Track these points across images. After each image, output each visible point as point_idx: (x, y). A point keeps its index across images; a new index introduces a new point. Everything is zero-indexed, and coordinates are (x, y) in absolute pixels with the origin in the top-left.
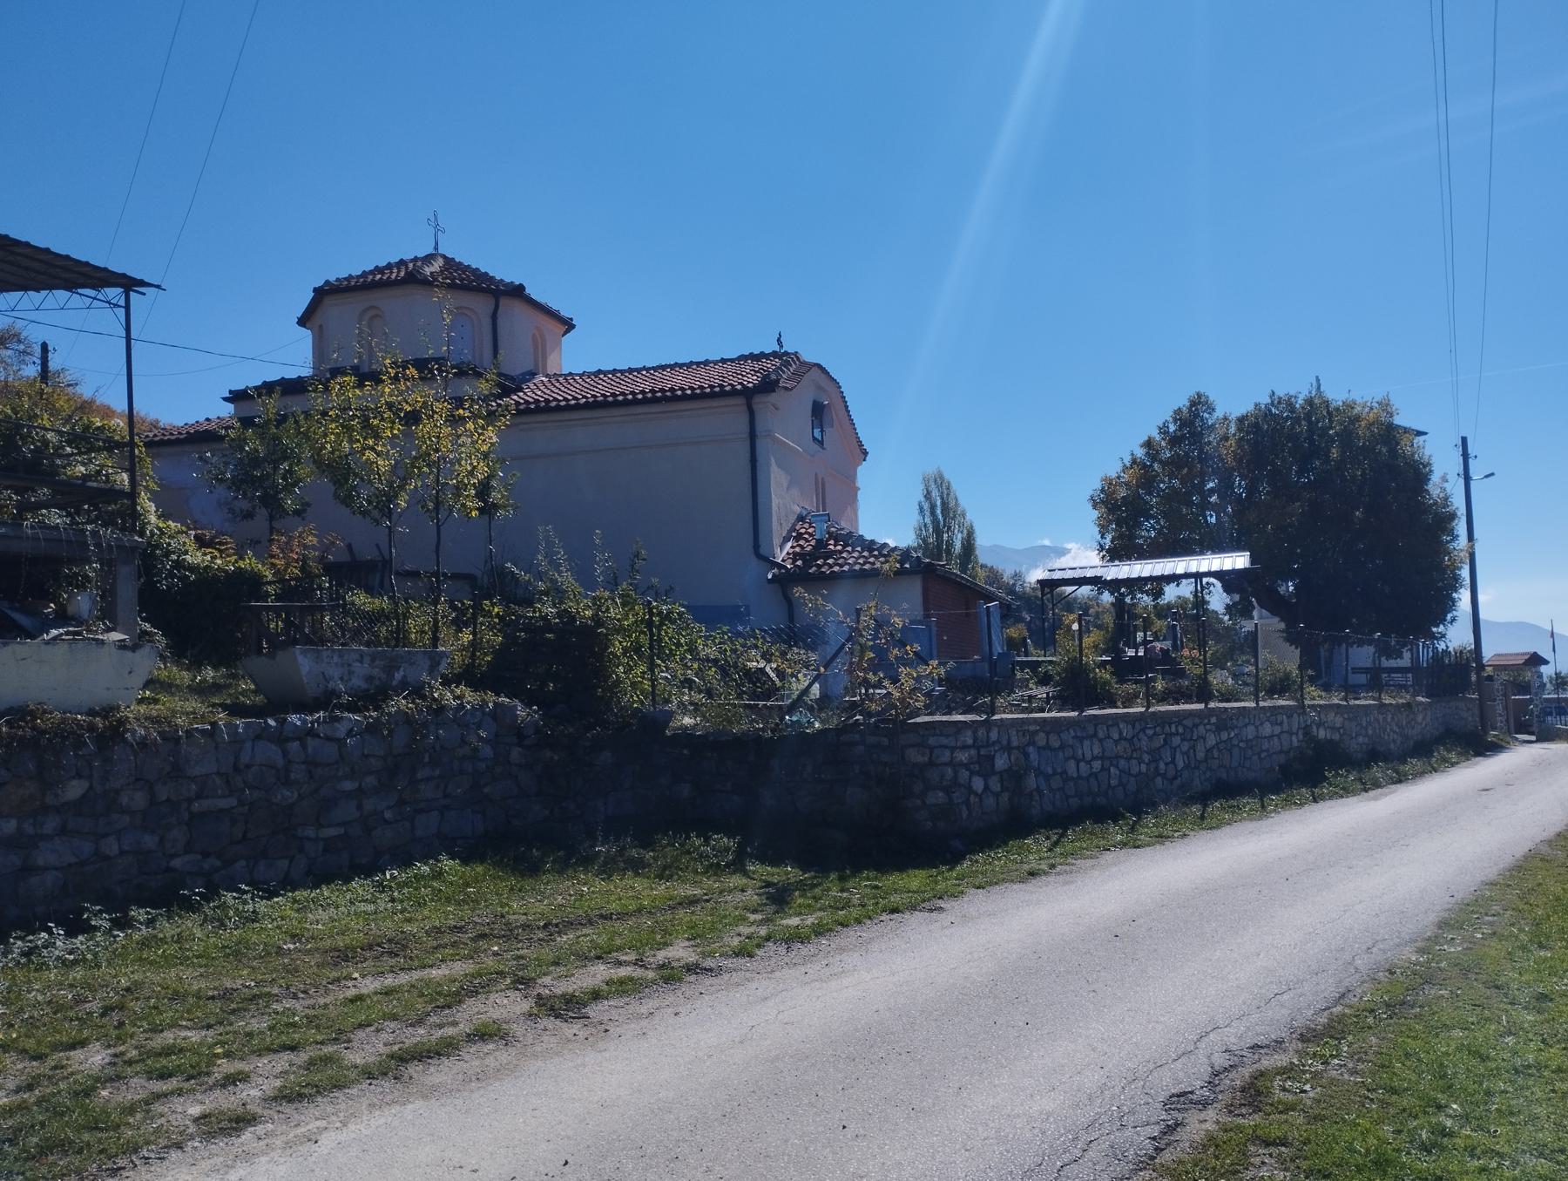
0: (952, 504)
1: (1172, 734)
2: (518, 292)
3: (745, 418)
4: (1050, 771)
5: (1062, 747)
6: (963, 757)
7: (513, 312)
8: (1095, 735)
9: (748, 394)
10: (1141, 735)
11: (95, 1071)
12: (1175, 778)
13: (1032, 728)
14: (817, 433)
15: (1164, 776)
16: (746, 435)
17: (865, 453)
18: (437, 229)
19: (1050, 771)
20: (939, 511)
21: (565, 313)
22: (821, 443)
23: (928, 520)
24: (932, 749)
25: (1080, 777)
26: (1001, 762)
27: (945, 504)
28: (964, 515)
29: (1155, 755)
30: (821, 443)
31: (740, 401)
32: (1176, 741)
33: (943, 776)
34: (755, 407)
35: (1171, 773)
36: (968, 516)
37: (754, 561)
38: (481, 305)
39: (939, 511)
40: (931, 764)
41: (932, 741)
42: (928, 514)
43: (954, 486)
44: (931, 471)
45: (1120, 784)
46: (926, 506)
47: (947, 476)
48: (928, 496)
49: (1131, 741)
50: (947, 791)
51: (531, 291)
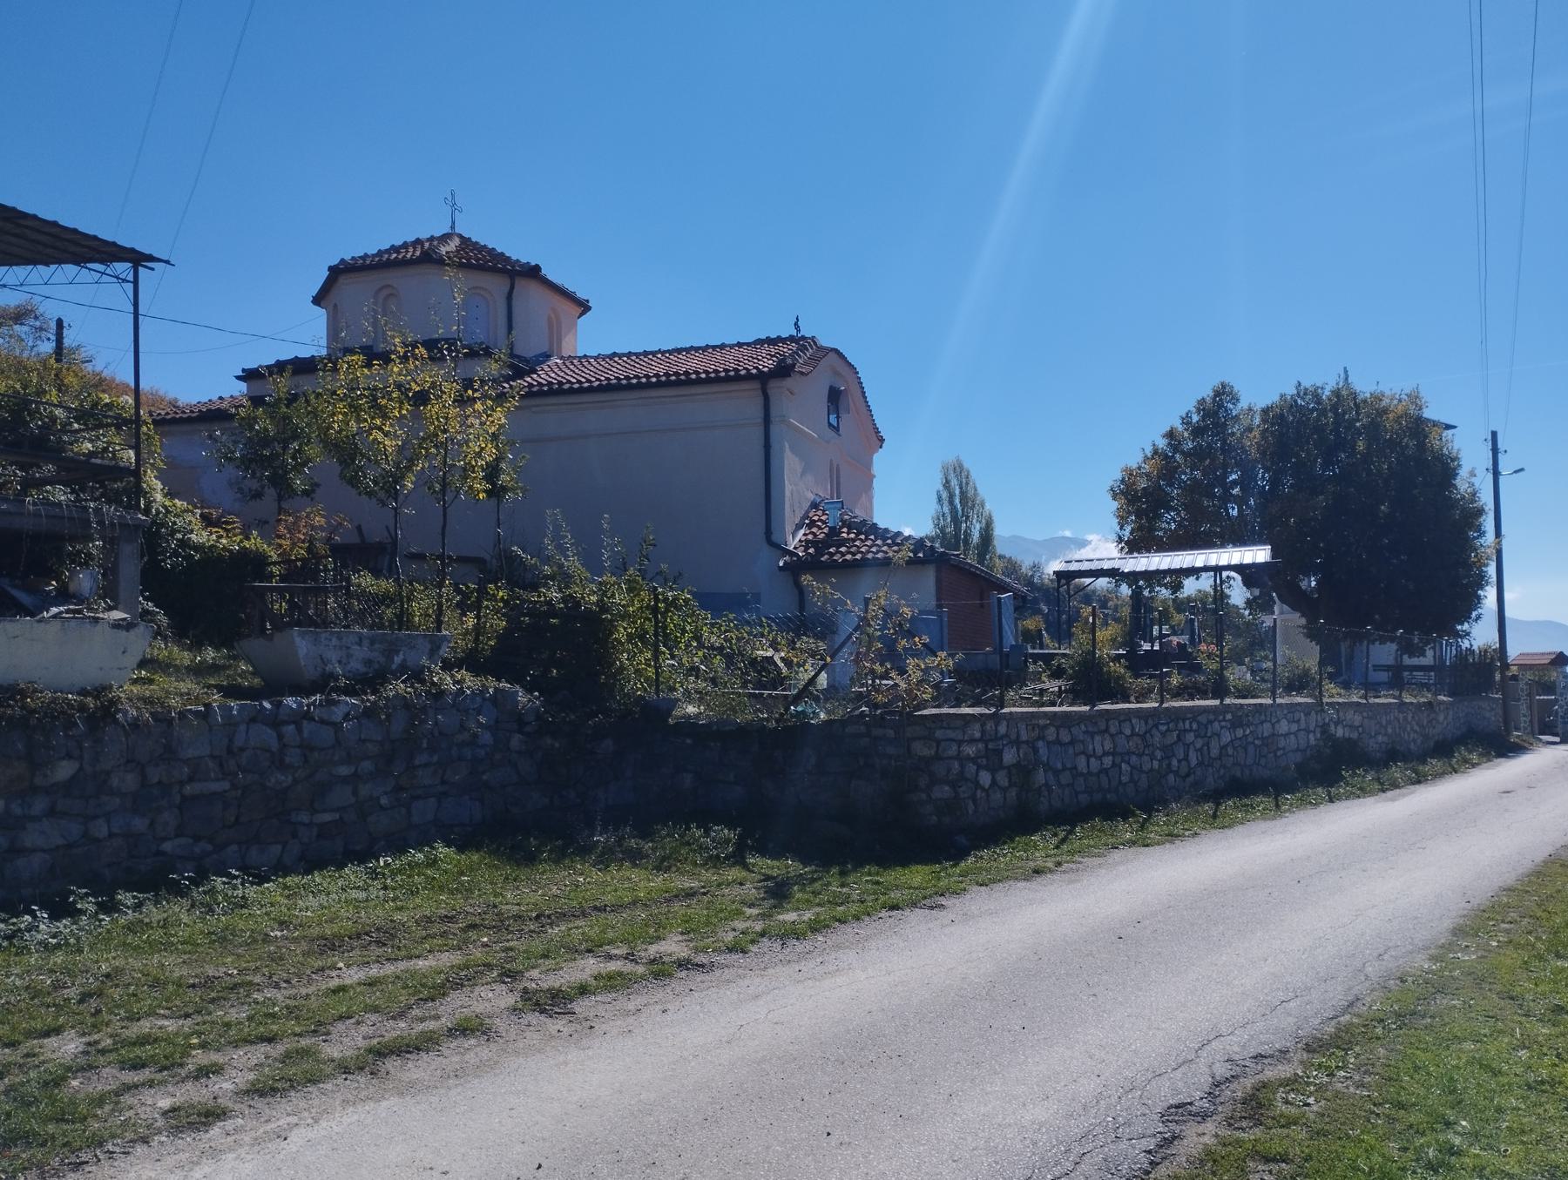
0: (971, 493)
2: (533, 272)
3: (760, 401)
6: (970, 750)
8: (1107, 730)
10: (1154, 731)
12: (1188, 775)
13: (1041, 722)
15: (1176, 773)
16: (760, 420)
17: (882, 440)
19: (1059, 766)
20: (957, 501)
21: (581, 295)
22: (836, 429)
23: (946, 509)
24: (938, 742)
25: (1090, 773)
27: (963, 494)
28: (982, 505)
30: (836, 429)
32: (1190, 737)
33: (949, 770)
35: (1184, 770)
36: (988, 506)
38: (495, 286)
39: (957, 501)
41: (939, 734)
42: (946, 503)
43: (973, 475)
44: (950, 459)
46: (945, 495)
47: (966, 465)
48: (947, 484)
49: (1143, 737)
50: (954, 785)
51: (546, 272)
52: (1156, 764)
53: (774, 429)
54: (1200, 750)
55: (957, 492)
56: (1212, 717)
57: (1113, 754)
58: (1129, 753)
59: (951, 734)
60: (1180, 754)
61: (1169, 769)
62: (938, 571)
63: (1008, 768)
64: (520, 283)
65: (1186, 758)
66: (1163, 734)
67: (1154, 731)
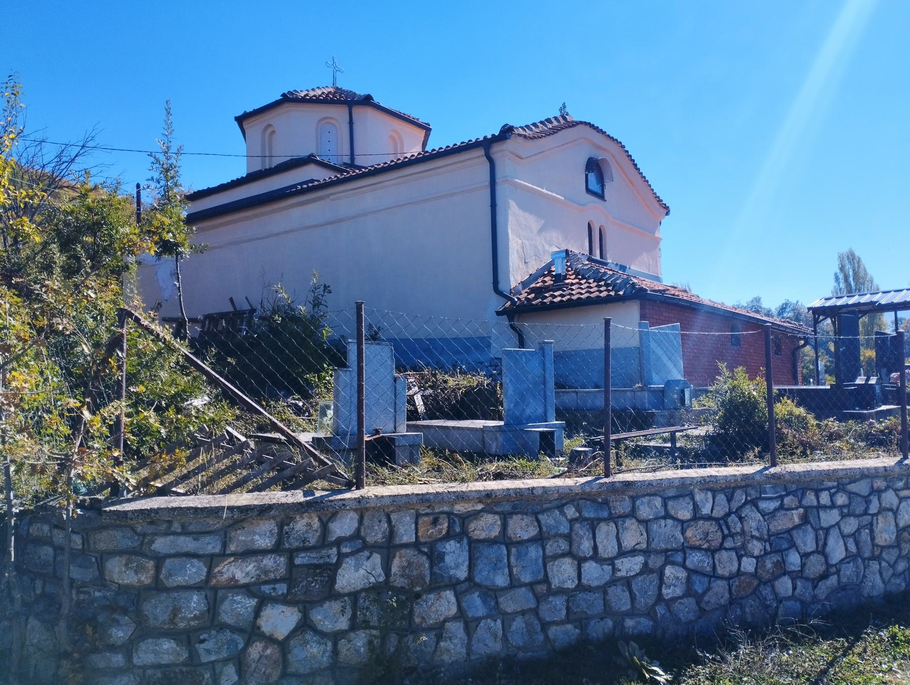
0: (862, 274)
1: (820, 507)
2: (367, 101)
3: (487, 166)
4: (501, 580)
5: (540, 539)
6: (241, 572)
7: (363, 114)
8: (633, 514)
9: (487, 144)
10: (747, 511)
11: (203, 607)
12: (824, 576)
13: (460, 508)
14: (594, 186)
15: (795, 576)
16: (488, 183)
17: (666, 208)
18: (336, 70)
19: (501, 580)
20: (851, 279)
21: (422, 120)
22: (601, 196)
23: (842, 285)
24: (159, 560)
25: (581, 587)
26: (353, 575)
27: (856, 274)
28: (872, 281)
29: (777, 544)
30: (601, 196)
31: (480, 152)
32: (829, 518)
33: (175, 612)
34: (494, 156)
35: (815, 566)
36: (876, 282)
37: (495, 297)
38: (339, 114)
39: (851, 279)
40: (158, 587)
41: (161, 545)
42: (842, 281)
43: (864, 261)
44: (845, 250)
45: (689, 592)
46: (841, 276)
47: (857, 254)
48: (842, 269)
49: (721, 522)
50: (188, 638)
51: (376, 99)
52: (749, 565)
53: (500, 189)
54: (855, 535)
55: (851, 273)
56: (880, 484)
57: (646, 552)
58: (686, 548)
59: (187, 544)
60: (807, 542)
61: (781, 569)
62: (642, 308)
63: (354, 596)
64: (358, 112)
65: (821, 550)
66: (769, 516)
67: (747, 511)
